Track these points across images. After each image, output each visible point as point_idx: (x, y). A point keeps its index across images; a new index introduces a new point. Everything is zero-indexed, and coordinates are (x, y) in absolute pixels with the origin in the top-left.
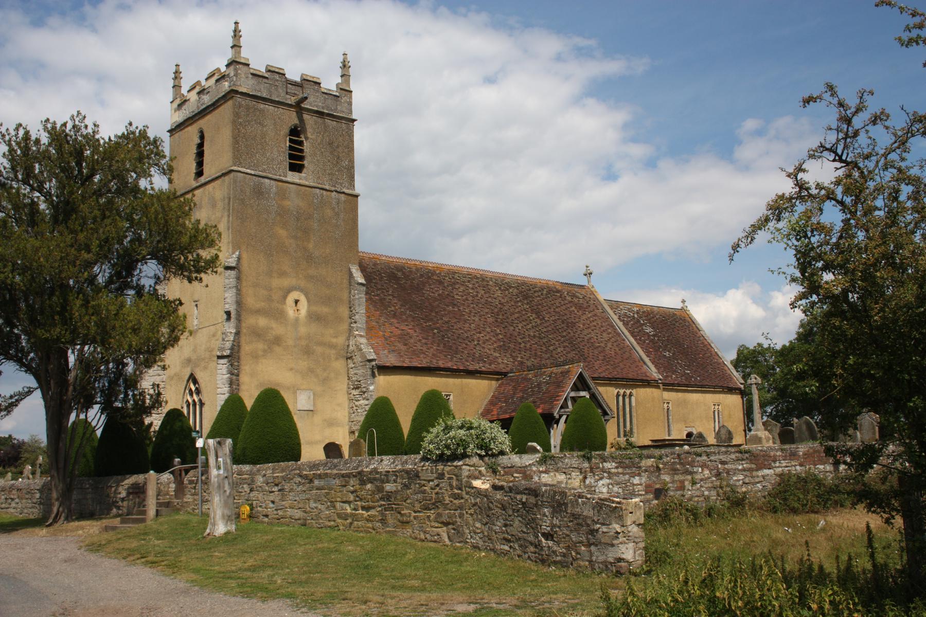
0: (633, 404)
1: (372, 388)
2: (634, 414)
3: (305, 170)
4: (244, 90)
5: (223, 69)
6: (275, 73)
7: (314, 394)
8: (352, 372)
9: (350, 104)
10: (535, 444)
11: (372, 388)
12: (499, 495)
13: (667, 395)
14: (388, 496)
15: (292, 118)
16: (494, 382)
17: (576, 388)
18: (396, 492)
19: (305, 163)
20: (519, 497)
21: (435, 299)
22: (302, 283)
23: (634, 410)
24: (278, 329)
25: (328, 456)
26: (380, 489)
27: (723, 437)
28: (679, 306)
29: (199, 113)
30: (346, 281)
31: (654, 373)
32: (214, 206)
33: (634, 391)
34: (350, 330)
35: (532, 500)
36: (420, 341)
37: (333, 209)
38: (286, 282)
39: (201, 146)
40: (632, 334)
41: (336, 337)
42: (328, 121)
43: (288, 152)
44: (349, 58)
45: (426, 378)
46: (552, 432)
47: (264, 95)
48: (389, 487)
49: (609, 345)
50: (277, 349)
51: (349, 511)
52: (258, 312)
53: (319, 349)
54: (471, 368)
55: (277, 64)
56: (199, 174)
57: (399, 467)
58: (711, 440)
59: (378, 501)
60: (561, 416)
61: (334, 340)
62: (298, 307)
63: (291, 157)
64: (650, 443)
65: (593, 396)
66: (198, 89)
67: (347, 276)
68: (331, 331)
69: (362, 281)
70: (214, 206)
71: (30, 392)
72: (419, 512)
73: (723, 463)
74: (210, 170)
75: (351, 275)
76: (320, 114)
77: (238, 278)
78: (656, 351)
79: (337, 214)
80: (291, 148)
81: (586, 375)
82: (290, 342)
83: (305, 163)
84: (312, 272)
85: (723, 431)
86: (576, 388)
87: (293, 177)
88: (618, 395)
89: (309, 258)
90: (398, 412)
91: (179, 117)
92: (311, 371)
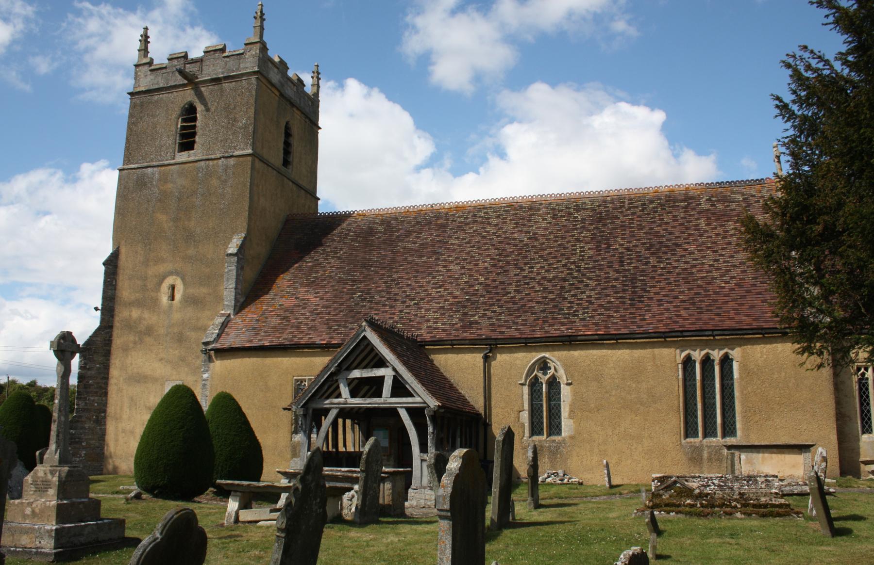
22: (169, 267)
24: (149, 318)
33: (736, 353)
37: (219, 178)
38: (162, 268)
42: (226, 85)
45: (280, 359)
50: (148, 340)
52: (131, 304)
63: (183, 136)
71: (863, 462)
76: (216, 81)
82: (162, 331)
84: (191, 252)
87: (183, 157)
88: (688, 363)
92: (183, 359)
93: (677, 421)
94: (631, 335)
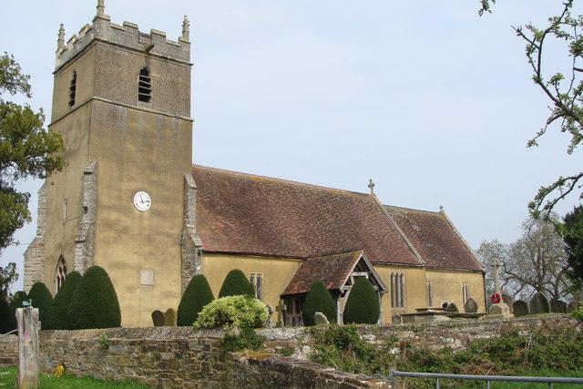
0: (404, 282)
1: (198, 268)
2: (404, 290)
3: (151, 100)
4: (106, 39)
5: (91, 24)
6: (130, 28)
7: (154, 273)
8: (185, 256)
9: (188, 53)
10: (321, 314)
11: (198, 268)
12: (255, 370)
13: (430, 275)
14: (163, 365)
15: (140, 62)
16: (296, 264)
17: (358, 269)
18: (171, 361)
19: (151, 94)
20: (271, 373)
21: (253, 202)
22: (140, 185)
23: (404, 287)
24: (126, 221)
25: (156, 324)
26: (158, 358)
27: (471, 308)
28: (438, 210)
29: (73, 58)
30: (181, 186)
31: (420, 259)
32: (80, 127)
34: (184, 223)
35: (283, 376)
36: (239, 232)
38: (133, 185)
39: (74, 82)
40: (404, 231)
41: (172, 228)
42: (171, 65)
43: (138, 86)
44: (189, 19)
46: (338, 303)
47: (121, 44)
48: (165, 356)
49: (386, 238)
51: (135, 375)
52: (110, 208)
53: (159, 238)
54: (278, 254)
55: (132, 21)
56: (72, 103)
57: (173, 338)
58: (461, 310)
59: (156, 368)
60: (346, 291)
61: (171, 231)
62: (142, 201)
63: (140, 90)
64: (416, 312)
65: (371, 275)
66: (74, 40)
67: (182, 182)
68: (169, 224)
69: (193, 185)
70: (80, 127)
72: (189, 380)
73: (473, 334)
74: (78, 101)
75: (185, 181)
77: (96, 182)
78: (422, 242)
79: (176, 135)
80: (140, 84)
81: (366, 259)
83: (151, 94)
84: (155, 178)
85: (470, 303)
86: (358, 269)
87: (140, 105)
89: (153, 168)
90: (211, 287)
91: (60, 63)
93: (420, 307)
94: (251, 254)
